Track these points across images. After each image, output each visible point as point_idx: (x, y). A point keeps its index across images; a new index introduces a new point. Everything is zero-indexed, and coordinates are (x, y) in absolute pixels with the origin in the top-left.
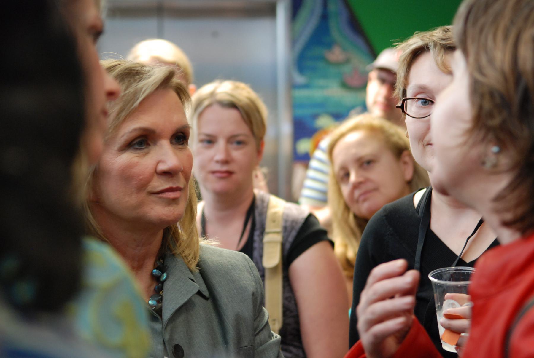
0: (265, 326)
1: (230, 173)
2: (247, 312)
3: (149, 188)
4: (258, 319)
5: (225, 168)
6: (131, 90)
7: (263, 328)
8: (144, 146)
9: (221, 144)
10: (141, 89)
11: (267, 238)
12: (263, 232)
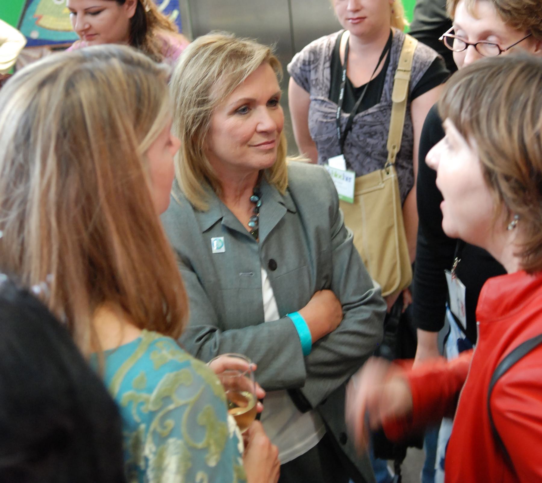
2: (324, 222)
3: (249, 143)
4: (335, 225)
5: (357, 15)
6: (239, 69)
7: (339, 232)
10: (246, 69)
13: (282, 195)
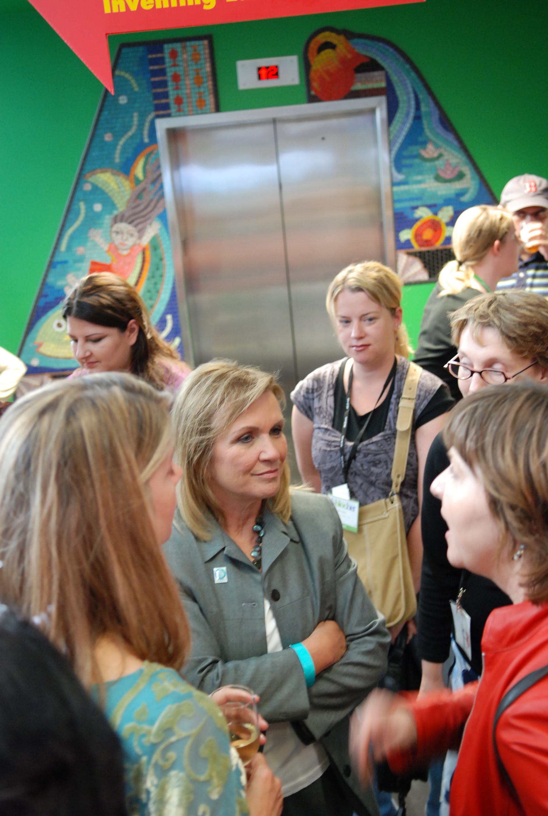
0: (345, 558)
1: (366, 346)
2: (328, 552)
3: (252, 472)
5: (361, 343)
6: (241, 397)
8: (249, 439)
9: (355, 322)
10: (248, 397)
11: (402, 403)
12: (399, 397)
13: (285, 525)
